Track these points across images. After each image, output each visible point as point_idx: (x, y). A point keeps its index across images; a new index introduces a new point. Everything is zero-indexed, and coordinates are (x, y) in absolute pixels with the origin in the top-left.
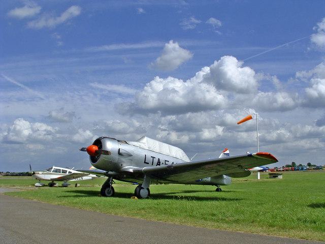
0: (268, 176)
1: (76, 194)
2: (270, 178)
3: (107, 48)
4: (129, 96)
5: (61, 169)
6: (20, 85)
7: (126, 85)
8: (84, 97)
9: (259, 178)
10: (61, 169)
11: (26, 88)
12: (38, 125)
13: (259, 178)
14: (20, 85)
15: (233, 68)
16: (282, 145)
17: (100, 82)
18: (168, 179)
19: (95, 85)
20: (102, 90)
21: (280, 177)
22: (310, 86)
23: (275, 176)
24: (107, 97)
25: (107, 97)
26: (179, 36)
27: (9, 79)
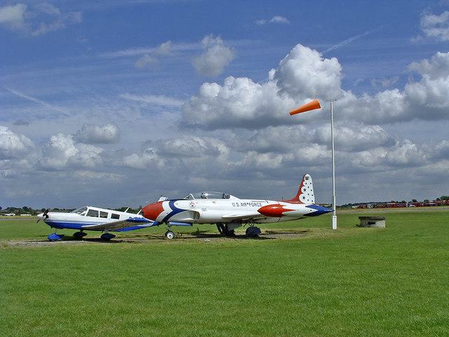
0: (359, 222)
2: (361, 226)
3: (123, 53)
4: (176, 109)
5: (99, 210)
6: (32, 99)
7: (167, 95)
8: (118, 112)
9: (335, 227)
10: (99, 210)
11: (42, 102)
12: (84, 147)
13: (335, 227)
14: (32, 99)
15: (311, 66)
16: (414, 170)
17: (132, 93)
18: (84, 237)
19: (127, 96)
20: (138, 103)
21: (381, 224)
22: (56, 135)
23: (370, 221)
24: (149, 111)
25: (149, 111)
26: (227, 35)
27: (17, 93)
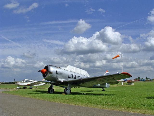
0: (127, 84)
1: (36, 92)
2: (128, 84)
3: (51, 23)
4: (61, 46)
5: (29, 80)
6: (9, 40)
7: (60, 40)
8: (40, 46)
9: (123, 85)
10: (29, 80)
11: (13, 42)
12: (18, 59)
13: (123, 85)
14: (9, 40)
15: (110, 33)
16: (133, 69)
17: (47, 39)
18: (79, 85)
19: (45, 40)
20: (48, 43)
21: (133, 84)
22: (147, 41)
23: (130, 84)
24: (51, 46)
25: (51, 46)
26: (85, 17)
27: (4, 38)
